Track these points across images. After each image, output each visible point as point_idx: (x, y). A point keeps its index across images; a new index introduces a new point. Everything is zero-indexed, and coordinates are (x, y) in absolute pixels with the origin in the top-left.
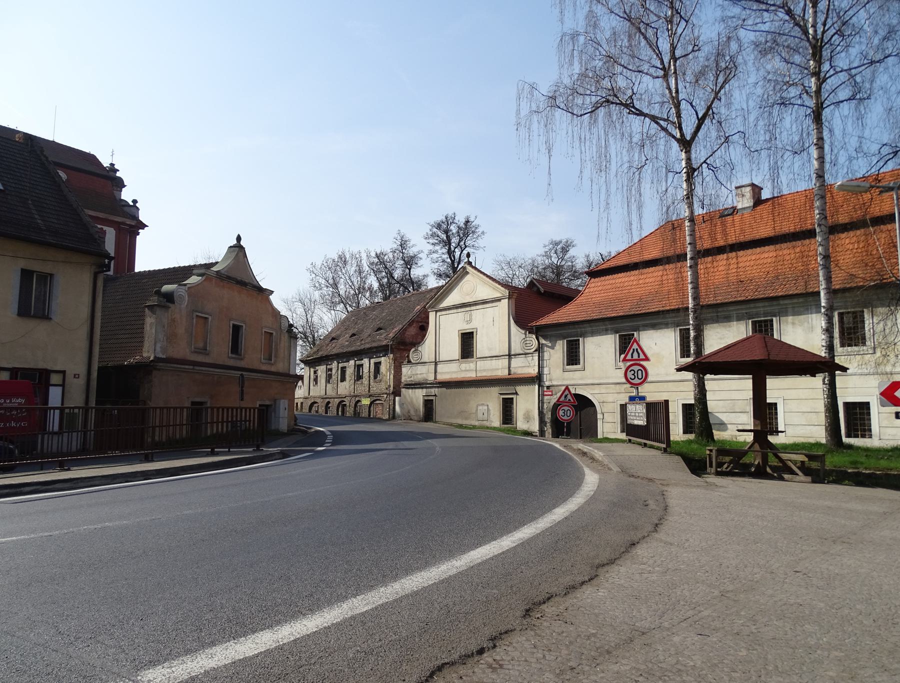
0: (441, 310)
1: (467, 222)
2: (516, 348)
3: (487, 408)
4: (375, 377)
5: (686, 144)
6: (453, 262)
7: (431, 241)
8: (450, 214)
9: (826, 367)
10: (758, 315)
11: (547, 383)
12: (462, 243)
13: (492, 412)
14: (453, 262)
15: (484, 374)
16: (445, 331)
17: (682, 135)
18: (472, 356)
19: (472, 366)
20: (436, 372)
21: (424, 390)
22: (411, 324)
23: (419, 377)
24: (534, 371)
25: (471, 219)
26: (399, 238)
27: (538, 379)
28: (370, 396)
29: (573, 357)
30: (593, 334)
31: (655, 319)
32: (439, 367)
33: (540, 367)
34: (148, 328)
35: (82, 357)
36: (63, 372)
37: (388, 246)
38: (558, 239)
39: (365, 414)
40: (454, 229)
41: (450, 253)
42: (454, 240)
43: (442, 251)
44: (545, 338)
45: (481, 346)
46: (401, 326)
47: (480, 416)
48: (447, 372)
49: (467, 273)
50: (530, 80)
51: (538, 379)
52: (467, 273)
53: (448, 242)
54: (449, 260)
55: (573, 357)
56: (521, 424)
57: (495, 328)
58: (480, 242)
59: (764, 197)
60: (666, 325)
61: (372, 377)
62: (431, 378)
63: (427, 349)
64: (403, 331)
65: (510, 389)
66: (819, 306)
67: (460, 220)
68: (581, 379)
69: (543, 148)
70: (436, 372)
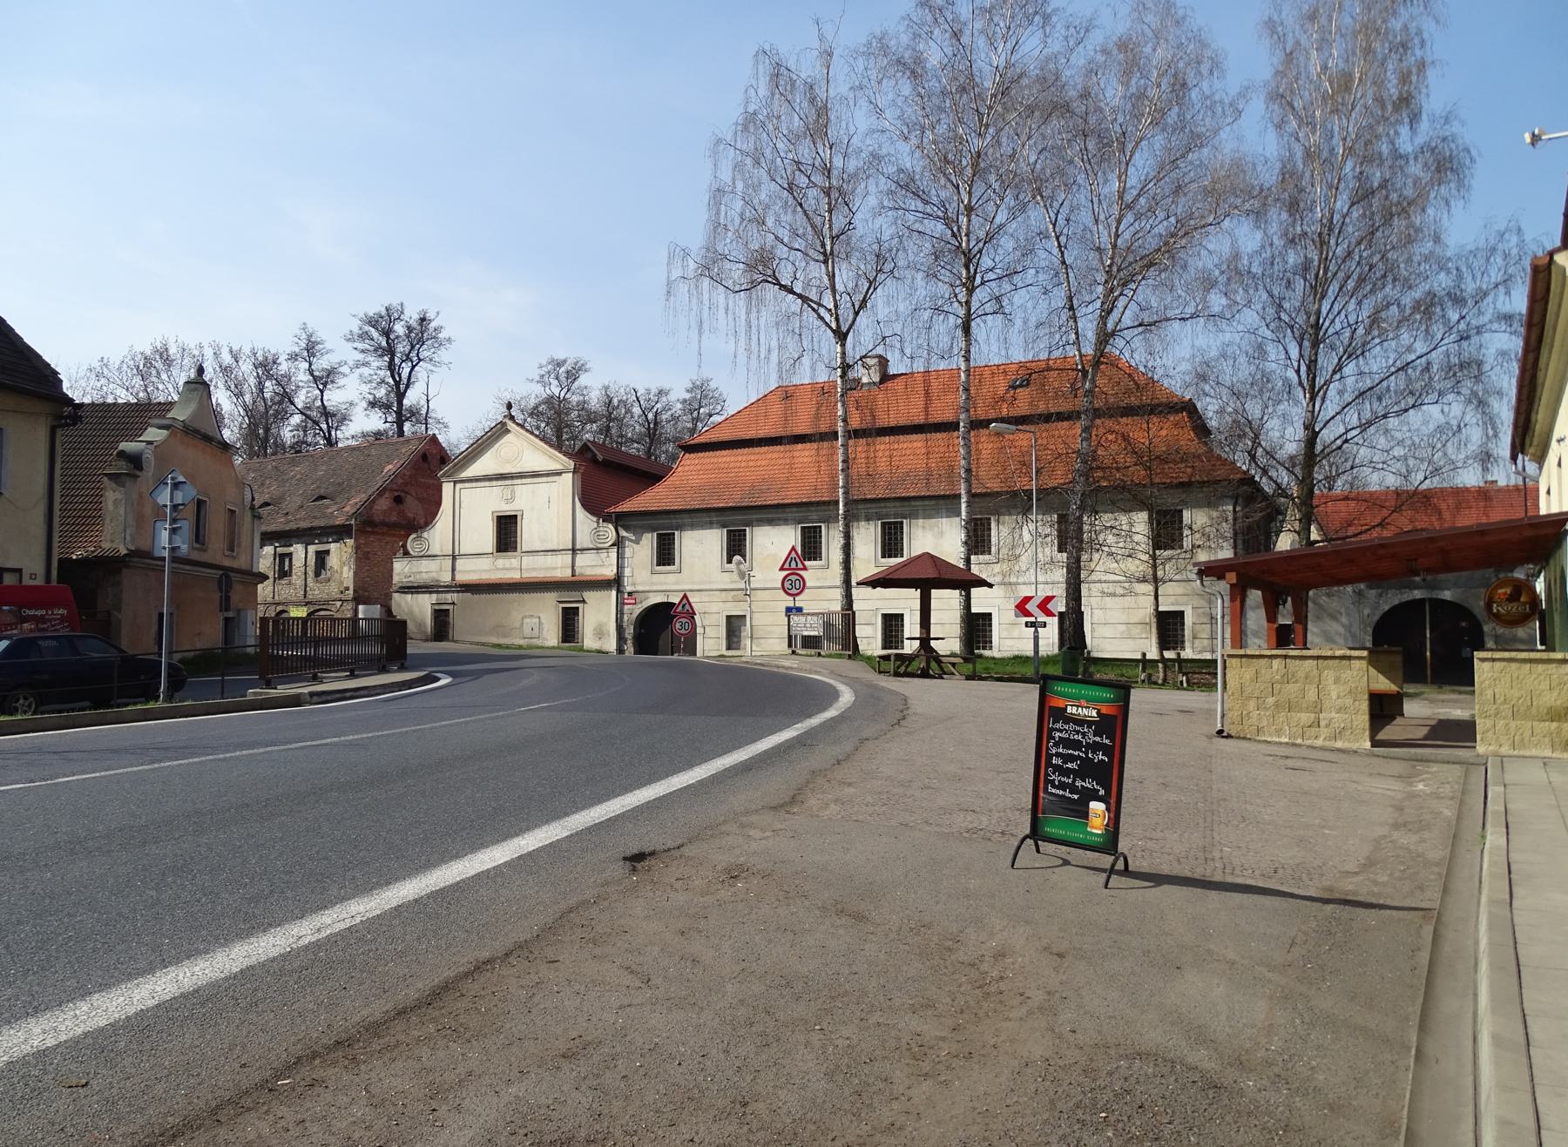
0: (462, 481)
1: (423, 320)
2: (583, 540)
3: (538, 623)
4: (317, 574)
5: (841, 336)
6: (397, 384)
7: (360, 346)
8: (395, 303)
9: (965, 583)
10: (887, 516)
11: (629, 589)
12: (413, 354)
13: (546, 627)
14: (397, 384)
15: (534, 574)
16: (466, 515)
17: (838, 326)
18: (515, 549)
19: (515, 562)
20: (453, 570)
21: (434, 596)
22: (381, 492)
23: (425, 576)
24: (610, 572)
25: (430, 315)
26: (304, 336)
27: (616, 582)
28: (307, 604)
29: (665, 556)
30: (693, 527)
31: (773, 513)
32: (459, 562)
33: (620, 567)
34: (111, 507)
35: (39, 549)
36: (19, 571)
37: (281, 343)
38: (560, 356)
39: (297, 631)
40: (399, 329)
41: (391, 367)
42: (402, 348)
43: (378, 364)
44: (627, 529)
45: (528, 534)
46: (364, 497)
47: (527, 631)
48: (470, 571)
49: (508, 431)
50: (683, 245)
51: (616, 582)
52: (508, 431)
53: (390, 351)
54: (391, 381)
55: (665, 556)
56: (589, 641)
57: (552, 511)
58: (443, 355)
59: (892, 370)
60: (786, 522)
61: (311, 573)
62: (446, 578)
63: (438, 536)
64: (370, 504)
65: (575, 596)
66: (959, 515)
67: (412, 315)
68: (677, 583)
69: (694, 325)
70: (453, 570)
